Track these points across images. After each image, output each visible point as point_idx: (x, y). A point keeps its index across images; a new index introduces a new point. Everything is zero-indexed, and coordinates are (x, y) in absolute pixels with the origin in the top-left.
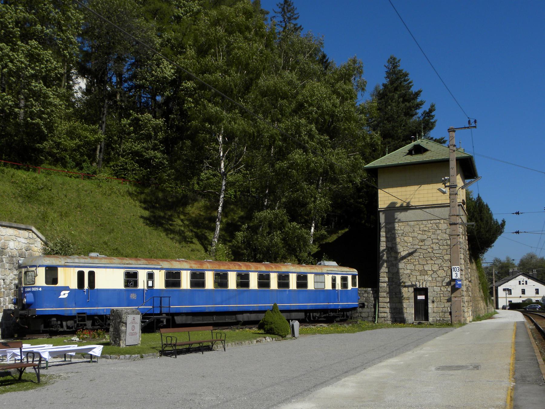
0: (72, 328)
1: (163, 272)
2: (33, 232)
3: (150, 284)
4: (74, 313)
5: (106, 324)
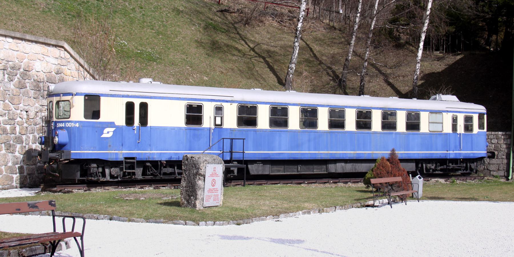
0: (117, 177)
1: (235, 106)
2: (66, 50)
3: (218, 122)
4: (121, 158)
5: (160, 174)
